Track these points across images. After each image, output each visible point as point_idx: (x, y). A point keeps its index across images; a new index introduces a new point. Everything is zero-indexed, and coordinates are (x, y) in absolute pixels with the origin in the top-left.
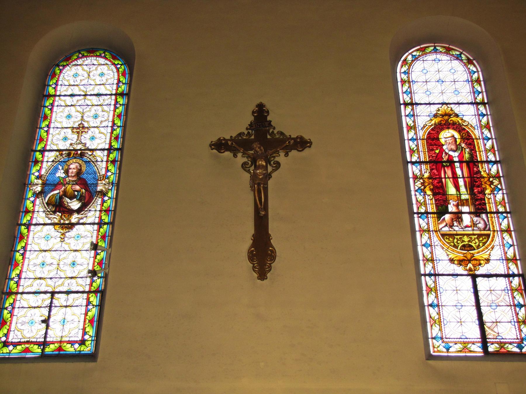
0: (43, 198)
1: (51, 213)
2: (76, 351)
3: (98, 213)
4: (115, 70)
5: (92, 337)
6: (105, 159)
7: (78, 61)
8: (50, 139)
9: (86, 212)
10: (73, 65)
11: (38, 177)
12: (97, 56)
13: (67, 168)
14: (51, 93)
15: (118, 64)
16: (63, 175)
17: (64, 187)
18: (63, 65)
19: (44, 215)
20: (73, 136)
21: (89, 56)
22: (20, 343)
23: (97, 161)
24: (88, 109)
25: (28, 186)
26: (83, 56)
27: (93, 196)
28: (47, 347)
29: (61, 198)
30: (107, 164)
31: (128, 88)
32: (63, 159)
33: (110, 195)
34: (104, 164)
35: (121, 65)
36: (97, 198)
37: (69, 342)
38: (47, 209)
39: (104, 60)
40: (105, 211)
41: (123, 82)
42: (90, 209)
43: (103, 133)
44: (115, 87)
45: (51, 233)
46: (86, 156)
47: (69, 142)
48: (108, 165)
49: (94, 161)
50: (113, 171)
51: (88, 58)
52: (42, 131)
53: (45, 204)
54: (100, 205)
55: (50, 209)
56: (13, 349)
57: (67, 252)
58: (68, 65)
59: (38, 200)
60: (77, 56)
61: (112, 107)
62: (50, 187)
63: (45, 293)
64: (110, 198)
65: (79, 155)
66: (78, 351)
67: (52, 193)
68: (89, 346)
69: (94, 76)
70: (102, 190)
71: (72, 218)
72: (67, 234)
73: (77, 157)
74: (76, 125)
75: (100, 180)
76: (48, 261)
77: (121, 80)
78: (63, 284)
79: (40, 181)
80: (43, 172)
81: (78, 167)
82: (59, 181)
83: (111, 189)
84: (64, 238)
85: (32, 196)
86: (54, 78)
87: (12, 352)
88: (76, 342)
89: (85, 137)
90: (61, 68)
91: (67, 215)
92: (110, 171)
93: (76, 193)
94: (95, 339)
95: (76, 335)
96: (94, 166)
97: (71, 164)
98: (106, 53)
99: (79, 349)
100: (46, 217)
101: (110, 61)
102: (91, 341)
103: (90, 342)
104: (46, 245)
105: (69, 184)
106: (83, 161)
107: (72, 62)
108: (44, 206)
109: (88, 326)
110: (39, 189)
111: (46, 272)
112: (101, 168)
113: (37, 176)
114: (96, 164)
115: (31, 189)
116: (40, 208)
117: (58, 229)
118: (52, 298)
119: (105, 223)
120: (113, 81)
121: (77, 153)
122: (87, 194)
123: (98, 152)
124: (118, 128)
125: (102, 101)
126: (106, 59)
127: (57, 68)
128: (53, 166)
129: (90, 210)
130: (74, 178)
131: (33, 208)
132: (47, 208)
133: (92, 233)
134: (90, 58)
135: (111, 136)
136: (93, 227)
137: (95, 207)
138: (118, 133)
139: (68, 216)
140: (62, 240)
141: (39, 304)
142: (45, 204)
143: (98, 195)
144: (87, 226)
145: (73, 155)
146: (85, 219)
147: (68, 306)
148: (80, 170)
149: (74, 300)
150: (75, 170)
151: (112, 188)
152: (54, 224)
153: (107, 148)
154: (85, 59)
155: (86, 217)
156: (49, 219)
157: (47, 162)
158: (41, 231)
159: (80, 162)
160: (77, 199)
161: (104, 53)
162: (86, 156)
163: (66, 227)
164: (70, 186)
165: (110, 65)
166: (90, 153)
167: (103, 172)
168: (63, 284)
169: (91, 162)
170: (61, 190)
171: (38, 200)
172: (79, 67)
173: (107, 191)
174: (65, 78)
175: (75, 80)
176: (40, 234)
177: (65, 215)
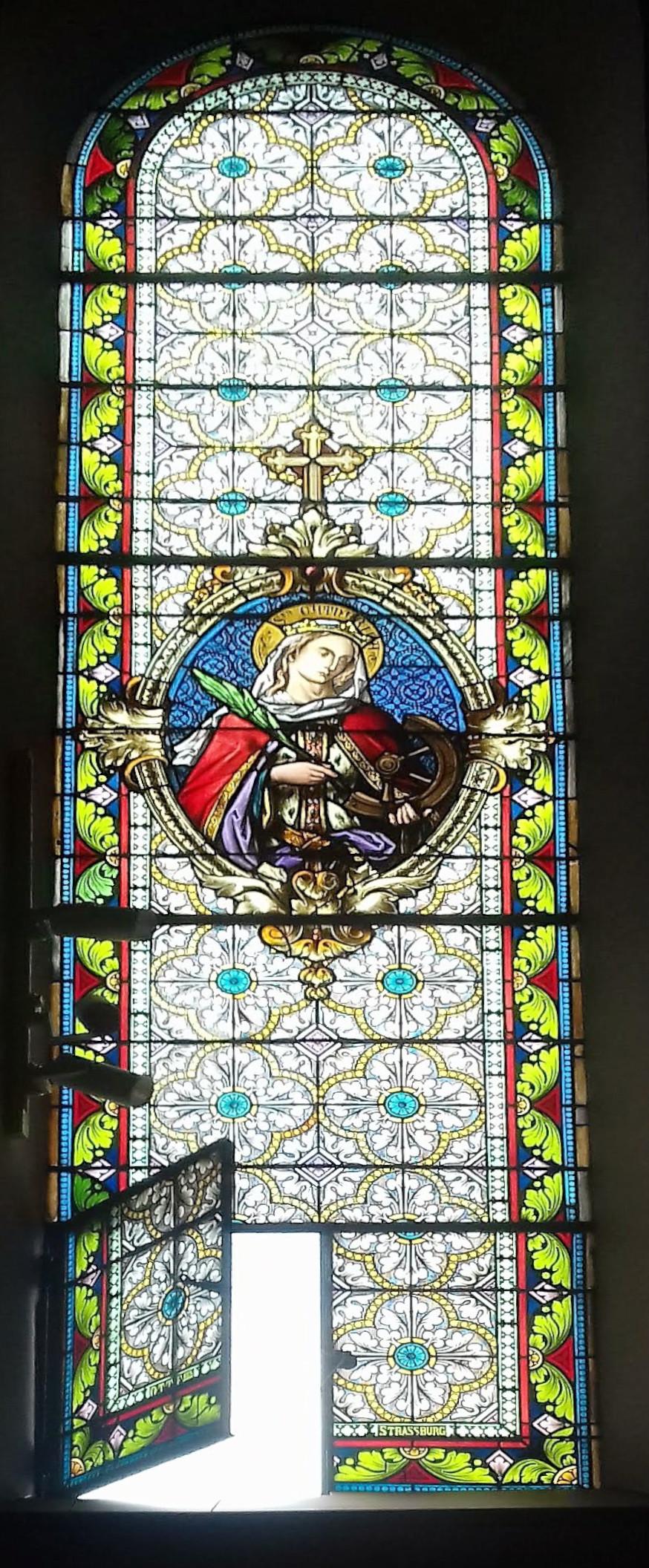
3: (491, 872)
7: (235, 89)
10: (205, 113)
12: (344, 68)
23: (441, 616)
30: (502, 630)
34: (486, 633)
49: (421, 613)
51: (291, 78)
60: (222, 61)
61: (508, 1308)
72: (340, 967)
84: (325, 985)
92: (537, 1152)
96: (428, 641)
98: (399, 52)
119: (542, 919)
124: (548, 1048)
126: (404, 84)
128: (188, 633)
134: (305, 77)
136: (471, 575)
140: (318, 997)
146: (424, 896)
156: (221, 893)
161: (387, 50)
169: (410, 620)
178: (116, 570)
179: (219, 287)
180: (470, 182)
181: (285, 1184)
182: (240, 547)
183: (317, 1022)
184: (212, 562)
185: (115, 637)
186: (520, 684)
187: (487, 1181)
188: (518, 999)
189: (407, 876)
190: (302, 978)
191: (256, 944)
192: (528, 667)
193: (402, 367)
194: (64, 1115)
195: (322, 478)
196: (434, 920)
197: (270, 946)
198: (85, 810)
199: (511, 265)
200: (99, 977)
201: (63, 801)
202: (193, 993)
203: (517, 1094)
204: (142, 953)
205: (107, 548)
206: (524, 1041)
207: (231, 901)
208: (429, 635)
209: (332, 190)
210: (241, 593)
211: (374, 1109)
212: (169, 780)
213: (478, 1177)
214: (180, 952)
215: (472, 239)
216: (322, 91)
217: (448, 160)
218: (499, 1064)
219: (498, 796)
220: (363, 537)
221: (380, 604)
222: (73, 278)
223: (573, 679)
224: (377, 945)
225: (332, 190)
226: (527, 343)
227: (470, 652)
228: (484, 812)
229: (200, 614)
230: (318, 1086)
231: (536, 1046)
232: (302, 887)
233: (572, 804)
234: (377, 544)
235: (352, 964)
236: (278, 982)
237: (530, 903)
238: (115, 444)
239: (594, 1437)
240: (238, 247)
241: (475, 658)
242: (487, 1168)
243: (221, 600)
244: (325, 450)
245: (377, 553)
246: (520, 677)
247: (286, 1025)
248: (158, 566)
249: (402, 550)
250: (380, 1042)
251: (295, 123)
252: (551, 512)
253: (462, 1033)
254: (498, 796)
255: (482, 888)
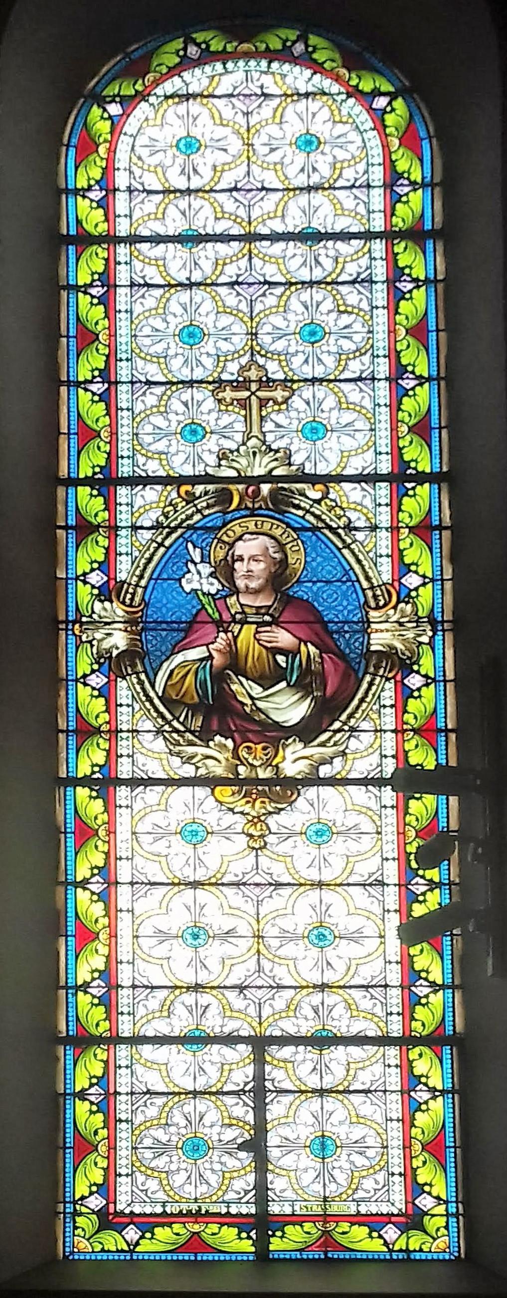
0: (143, 677)
1: (189, 736)
2: (391, 1251)
3: (389, 742)
4: (365, 120)
5: (446, 1202)
6: (384, 518)
7: (186, 75)
8: (125, 432)
9: (339, 736)
11: (105, 593)
12: (271, 55)
13: (221, 554)
14: (89, 228)
15: (377, 93)
16: (213, 587)
17: (222, 635)
18: (118, 95)
19: (160, 744)
20: (226, 419)
21: (235, 56)
22: (166, 1219)
23: (349, 528)
24: (271, 301)
25: (67, 630)
26: (207, 57)
27: (356, 672)
28: (274, 1235)
29: (220, 678)
30: (395, 540)
31: (438, 205)
32: (197, 517)
33: (427, 664)
34: (384, 539)
35: (393, 96)
36: (135, 579)
37: (357, 1219)
38: (169, 723)
39: (308, 73)
40: (94, 528)
41: (412, 178)
42: (352, 722)
43: (358, 408)
44: (377, 199)
45: (204, 817)
46: (298, 507)
47: (212, 443)
48: (402, 545)
49: (335, 525)
50: (426, 568)
52: (84, 397)
53: (157, 701)
54: (392, 706)
55: (182, 724)
56: (142, 1237)
57: (286, 892)
58: (142, 96)
59: (122, 684)
61: (380, 295)
62: (164, 633)
63: (230, 1040)
64: (429, 680)
65: (264, 499)
66: (401, 1251)
67: (179, 658)
68: (439, 1234)
69: (272, 150)
70: (392, 647)
71: (284, 758)
72: (272, 821)
73: (260, 508)
74: (232, 370)
75: (378, 608)
76: (216, 921)
77: (402, 166)
78: (292, 1009)
79: (119, 611)
80: (124, 569)
81: (271, 550)
82: (199, 612)
83: (432, 644)
84: (262, 836)
85: (96, 667)
86: (91, 158)
87: (138, 1249)
88: (388, 1218)
89: (278, 425)
90: (114, 109)
91: (259, 747)
92: (413, 568)
93: (281, 659)
94: (461, 1211)
95: (379, 1193)
96: (339, 549)
97: (240, 538)
99: (401, 1244)
100: (171, 753)
101: (338, 79)
102: (445, 1219)
103: (442, 1221)
104: (191, 861)
105: (243, 622)
106: (288, 525)
107: (157, 83)
108: (157, 710)
109: (424, 1163)
110: (119, 640)
111: (215, 967)
112: (371, 554)
113: (413, 671)
114: (349, 541)
115: (84, 638)
116: (138, 716)
117: (231, 799)
118: (259, 1061)
120: (366, 172)
121: (257, 492)
122: (328, 666)
123: (347, 486)
125: (328, 264)
126: (317, 68)
127: (96, 111)
128: (161, 545)
129: (353, 729)
130: (261, 596)
131: (106, 717)
132: (169, 716)
133: (376, 818)
135: (394, 424)
137: (375, 716)
138: (424, 409)
139: (264, 749)
141: (211, 1078)
142: (157, 701)
143: (377, 667)
144: (351, 788)
145: (241, 500)
147: (330, 1091)
148: (284, 563)
149: (348, 1071)
150: (262, 565)
151: (432, 638)
152: (211, 782)
153: (385, 472)
154: (219, 66)
155: (344, 754)
157: (135, 528)
158: (345, 455)
159: (277, 532)
160: (288, 685)
162: (298, 507)
163: (262, 794)
164: (248, 631)
165: (339, 98)
166: (314, 493)
167: (385, 572)
168: (292, 1009)
169: (326, 532)
170: (211, 646)
171: (122, 684)
172: (194, 107)
173: (412, 652)
174: (140, 158)
175: (189, 169)
176: (157, 818)
177: (249, 748)
178: (104, 490)
179: (179, 246)
180: (370, 153)
181: (233, 1108)
182: (200, 470)
183: (260, 1004)
184: (178, 481)
185: (104, 547)
186: (412, 687)
187: (374, 390)
188: (415, 1163)
189: (325, 746)
190: (246, 831)
191: (211, 802)
192: (416, 572)
193: (329, 916)
194: (68, 1102)
195: (261, 410)
196: (346, 782)
197: (221, 803)
198: (84, 693)
199: (401, 224)
200: (95, 431)
201: (65, 1218)
202: (165, 1159)
203: (396, 324)
204: (123, 729)
205: (100, 473)
206: (416, 986)
207: (193, 767)
208: (340, 545)
209: (276, 959)
210: (199, 511)
211: (295, 434)
212: (145, 667)
213: (361, 193)
214: (157, 1015)
215: (383, 799)
216: (256, 75)
217: (353, 136)
218: (387, 547)
219: (392, 681)
220: (292, 459)
221: (303, 517)
222: (68, 1040)
223: (439, 139)
224: (301, 803)
225: (276, 959)
226: (421, 589)
227: (372, 559)
228: (382, 694)
229: (168, 526)
230: (252, 319)
231: (406, 190)
232: (246, 756)
233: (448, 585)
234: (303, 464)
235: (284, 819)
236: (226, 834)
237: (413, 465)
238: (102, 578)
239: (442, 378)
240: (195, 407)
241: (375, 565)
242: (386, 986)
243: (183, 516)
244: (263, 402)
245: (303, 472)
246: (412, 681)
247: (235, 1188)
248: (137, 485)
249: (322, 469)
250: (294, 190)
251: (238, 294)
252: (442, 739)
253: (355, 276)
254: (392, 681)
255: (372, 259)
